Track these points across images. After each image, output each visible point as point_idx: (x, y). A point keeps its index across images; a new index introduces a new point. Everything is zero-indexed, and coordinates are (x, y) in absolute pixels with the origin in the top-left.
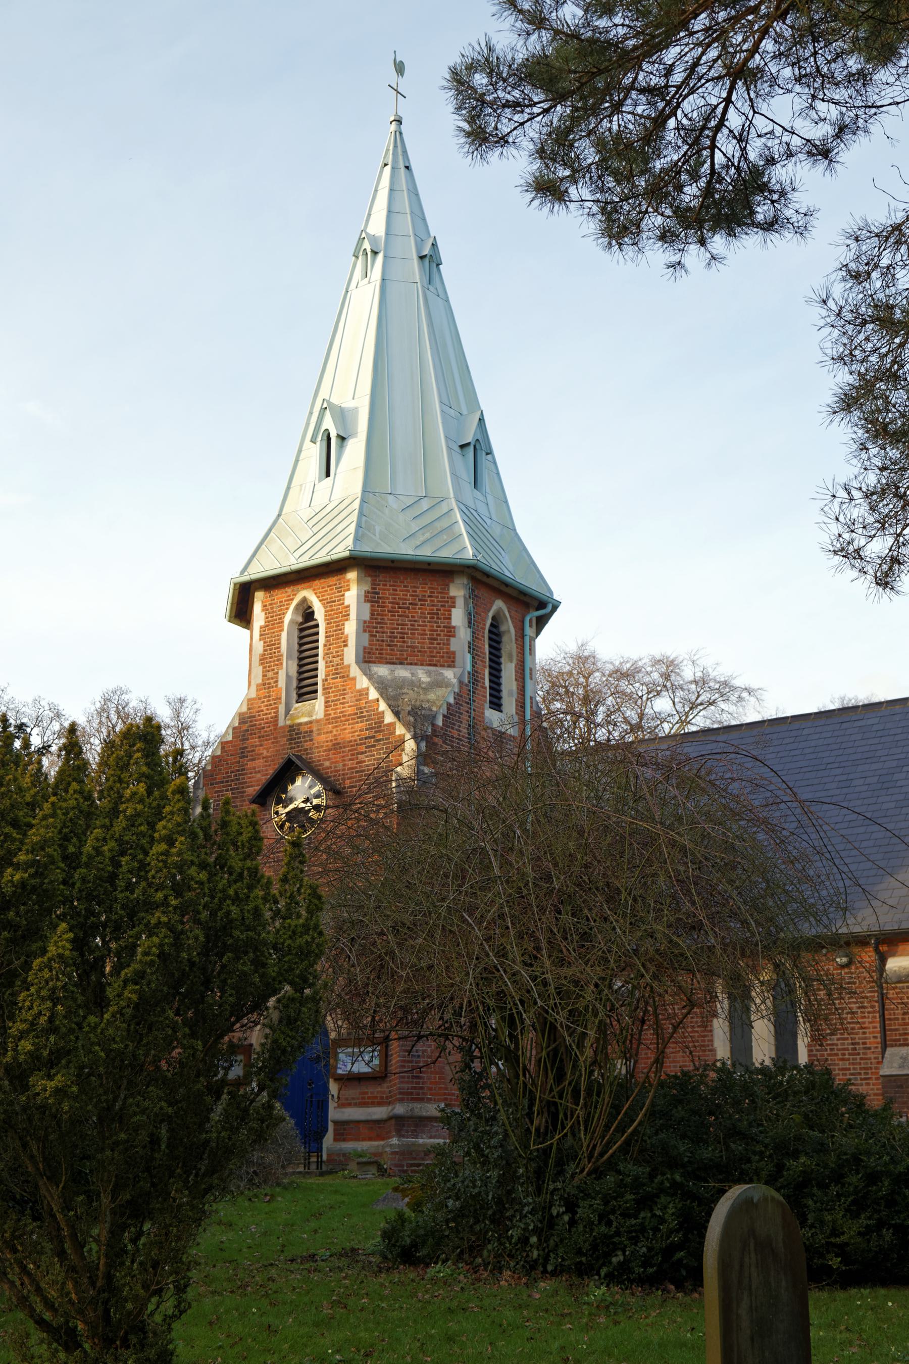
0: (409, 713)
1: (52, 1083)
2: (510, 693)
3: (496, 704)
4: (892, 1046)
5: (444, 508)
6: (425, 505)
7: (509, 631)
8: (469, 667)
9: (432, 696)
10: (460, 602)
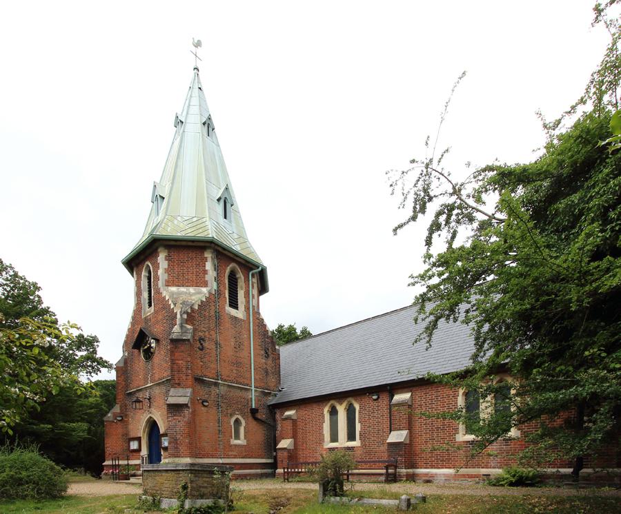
0: (181, 304)
1: (33, 456)
2: (242, 302)
3: (234, 304)
4: (394, 430)
5: (204, 220)
6: (195, 219)
7: (240, 277)
8: (215, 287)
9: (193, 298)
10: (209, 259)
